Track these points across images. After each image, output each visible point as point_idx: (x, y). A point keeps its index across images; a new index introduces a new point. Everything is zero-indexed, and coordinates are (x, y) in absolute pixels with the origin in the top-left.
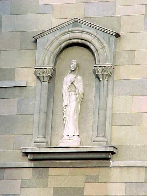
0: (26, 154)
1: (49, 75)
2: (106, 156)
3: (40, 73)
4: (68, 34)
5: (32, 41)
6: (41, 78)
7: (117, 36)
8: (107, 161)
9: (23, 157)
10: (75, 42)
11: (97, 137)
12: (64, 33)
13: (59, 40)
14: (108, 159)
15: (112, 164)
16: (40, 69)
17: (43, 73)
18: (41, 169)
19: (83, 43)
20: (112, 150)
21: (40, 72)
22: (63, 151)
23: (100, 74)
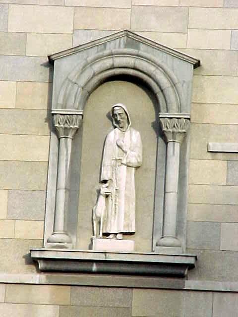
0: (34, 262)
1: (75, 126)
2: (171, 271)
3: (60, 123)
4: (134, 59)
5: (42, 63)
6: (61, 132)
7: (51, 63)
8: (180, 281)
9: (27, 266)
10: (116, 73)
11: (53, 234)
12: (148, 59)
13: (156, 73)
14: (182, 276)
15: (190, 284)
16: (61, 114)
17: (66, 122)
18: (102, 289)
19: (140, 77)
20: (191, 261)
21: (168, 125)
22: (151, 261)
23: (170, 131)
